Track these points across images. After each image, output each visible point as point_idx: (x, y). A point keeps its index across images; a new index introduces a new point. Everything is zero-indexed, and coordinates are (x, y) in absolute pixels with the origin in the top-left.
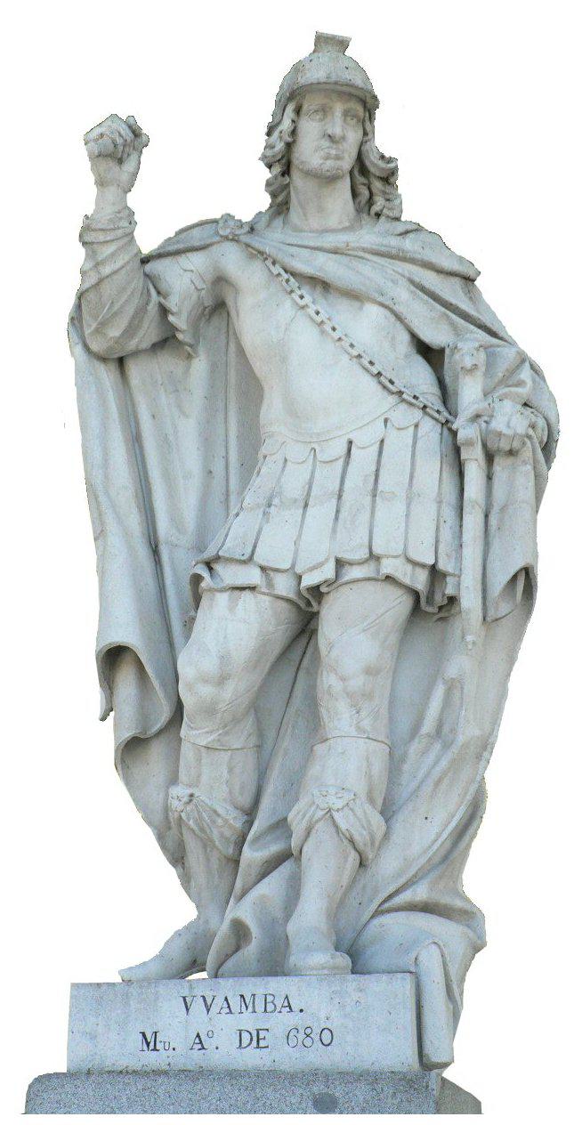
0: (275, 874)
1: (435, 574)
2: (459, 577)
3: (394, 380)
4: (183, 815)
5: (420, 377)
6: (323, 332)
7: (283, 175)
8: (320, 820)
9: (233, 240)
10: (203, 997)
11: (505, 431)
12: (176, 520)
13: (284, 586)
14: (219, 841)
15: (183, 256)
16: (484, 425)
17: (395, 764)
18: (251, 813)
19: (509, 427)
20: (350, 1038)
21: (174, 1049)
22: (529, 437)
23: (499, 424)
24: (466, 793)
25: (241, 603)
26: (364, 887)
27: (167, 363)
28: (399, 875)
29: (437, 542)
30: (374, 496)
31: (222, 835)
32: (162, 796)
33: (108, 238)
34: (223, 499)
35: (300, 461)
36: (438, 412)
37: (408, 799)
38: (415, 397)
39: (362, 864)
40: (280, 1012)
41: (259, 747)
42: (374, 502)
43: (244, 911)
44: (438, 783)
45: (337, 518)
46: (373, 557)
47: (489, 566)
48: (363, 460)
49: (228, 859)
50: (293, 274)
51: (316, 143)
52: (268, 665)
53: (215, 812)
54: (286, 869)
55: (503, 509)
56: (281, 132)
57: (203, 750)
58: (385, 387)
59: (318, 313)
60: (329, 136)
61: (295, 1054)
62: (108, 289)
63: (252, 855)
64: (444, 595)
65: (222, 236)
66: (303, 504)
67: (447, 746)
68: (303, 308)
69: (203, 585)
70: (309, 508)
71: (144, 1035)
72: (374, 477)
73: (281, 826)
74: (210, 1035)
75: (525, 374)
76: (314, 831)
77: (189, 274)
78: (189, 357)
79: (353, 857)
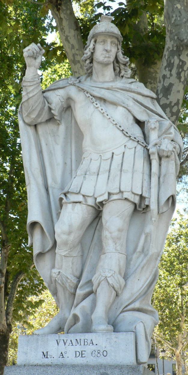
0: (88, 298)
1: (142, 197)
2: (150, 198)
5: (137, 131)
6: (104, 116)
7: (90, 63)
9: (73, 85)
10: (63, 340)
11: (165, 149)
13: (91, 201)
15: (57, 90)
16: (158, 147)
17: (128, 262)
18: (79, 278)
20: (113, 354)
21: (53, 358)
23: (163, 147)
26: (118, 303)
27: (51, 126)
29: (142, 187)
31: (70, 286)
32: (49, 272)
36: (143, 143)
37: (133, 273)
38: (135, 138)
39: (117, 295)
40: (89, 345)
43: (77, 311)
45: (108, 179)
46: (121, 192)
47: (160, 195)
48: (117, 159)
49: (72, 294)
50: (94, 97)
53: (67, 277)
54: (91, 297)
55: (165, 176)
56: (90, 49)
57: (63, 257)
58: (125, 135)
59: (102, 110)
61: (94, 359)
63: (80, 292)
65: (69, 84)
66: (97, 174)
67: (146, 255)
68: (97, 108)
69: (63, 201)
71: (43, 353)
72: (121, 165)
74: (66, 353)
76: (101, 284)
78: (59, 124)
79: (114, 293)
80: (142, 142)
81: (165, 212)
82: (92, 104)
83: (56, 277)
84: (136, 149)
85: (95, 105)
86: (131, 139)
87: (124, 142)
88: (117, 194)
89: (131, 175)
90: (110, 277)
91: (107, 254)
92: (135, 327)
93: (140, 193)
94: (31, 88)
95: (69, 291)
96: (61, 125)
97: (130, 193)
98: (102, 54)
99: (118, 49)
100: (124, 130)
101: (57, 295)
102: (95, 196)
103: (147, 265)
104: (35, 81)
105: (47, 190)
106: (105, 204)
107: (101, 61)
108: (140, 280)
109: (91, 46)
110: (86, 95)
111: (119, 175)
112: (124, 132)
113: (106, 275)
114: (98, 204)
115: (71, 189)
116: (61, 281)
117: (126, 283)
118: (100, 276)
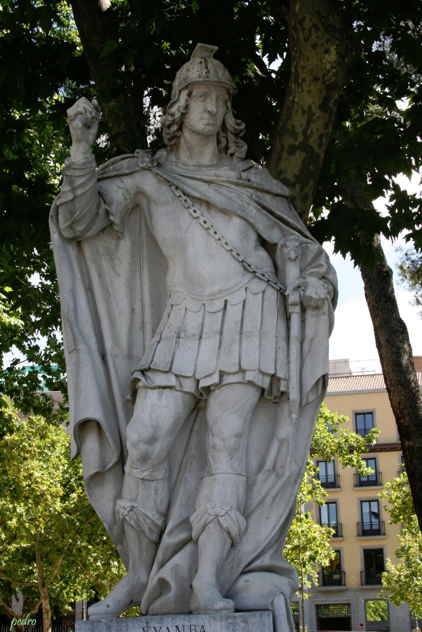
0: (183, 551)
2: (288, 380)
3: (251, 264)
4: (127, 518)
6: (209, 234)
7: (178, 130)
8: (211, 522)
9: (148, 169)
10: (154, 627)
11: (314, 296)
12: (116, 340)
13: (189, 385)
14: (149, 532)
16: (302, 292)
17: (249, 487)
18: (166, 516)
19: (316, 293)
22: (327, 299)
23: (310, 292)
24: (288, 503)
25: (164, 396)
26: (234, 558)
27: (108, 241)
28: (254, 551)
29: (276, 360)
30: (241, 334)
31: (150, 529)
32: (112, 505)
33: (81, 174)
34: (141, 326)
35: (196, 311)
36: (276, 284)
38: (263, 275)
39: (233, 545)
41: (170, 478)
42: (241, 338)
43: (166, 573)
44: (274, 498)
45: (220, 347)
46: (242, 371)
47: (304, 374)
48: (234, 312)
49: (152, 542)
50: (188, 196)
51: (200, 116)
52: (178, 430)
53: (147, 516)
54: (188, 548)
55: (311, 340)
56: (179, 107)
57: (140, 481)
58: (234, 258)
59: (205, 222)
60: (209, 111)
62: (78, 204)
64: (279, 390)
66: (198, 338)
67: (279, 476)
68: (196, 218)
69: (140, 384)
70: (202, 340)
72: (240, 322)
73: (185, 523)
75: (322, 261)
76: (207, 528)
77: (121, 190)
78: (119, 238)
79: (229, 542)
80: (275, 282)
81: (311, 402)
82: (186, 210)
83: (126, 516)
84: (265, 295)
85: (193, 213)
86: (256, 276)
87: (245, 283)
88: (234, 374)
89: (258, 342)
90: (224, 515)
91: (216, 476)
92: (272, 602)
93: (273, 372)
94: (80, 181)
95: (148, 538)
96: (123, 239)
97: (257, 372)
98: (201, 119)
99: (227, 108)
100: (245, 260)
101: (122, 543)
102: (196, 375)
103: (281, 493)
104: (87, 168)
105: (104, 357)
106: (214, 390)
107: (200, 131)
108: (269, 519)
109: (182, 102)
110: (174, 194)
111: (238, 341)
112: (244, 264)
113: (217, 513)
114: (201, 391)
115: (153, 363)
116: (135, 521)
117: (247, 523)
118: (205, 514)
